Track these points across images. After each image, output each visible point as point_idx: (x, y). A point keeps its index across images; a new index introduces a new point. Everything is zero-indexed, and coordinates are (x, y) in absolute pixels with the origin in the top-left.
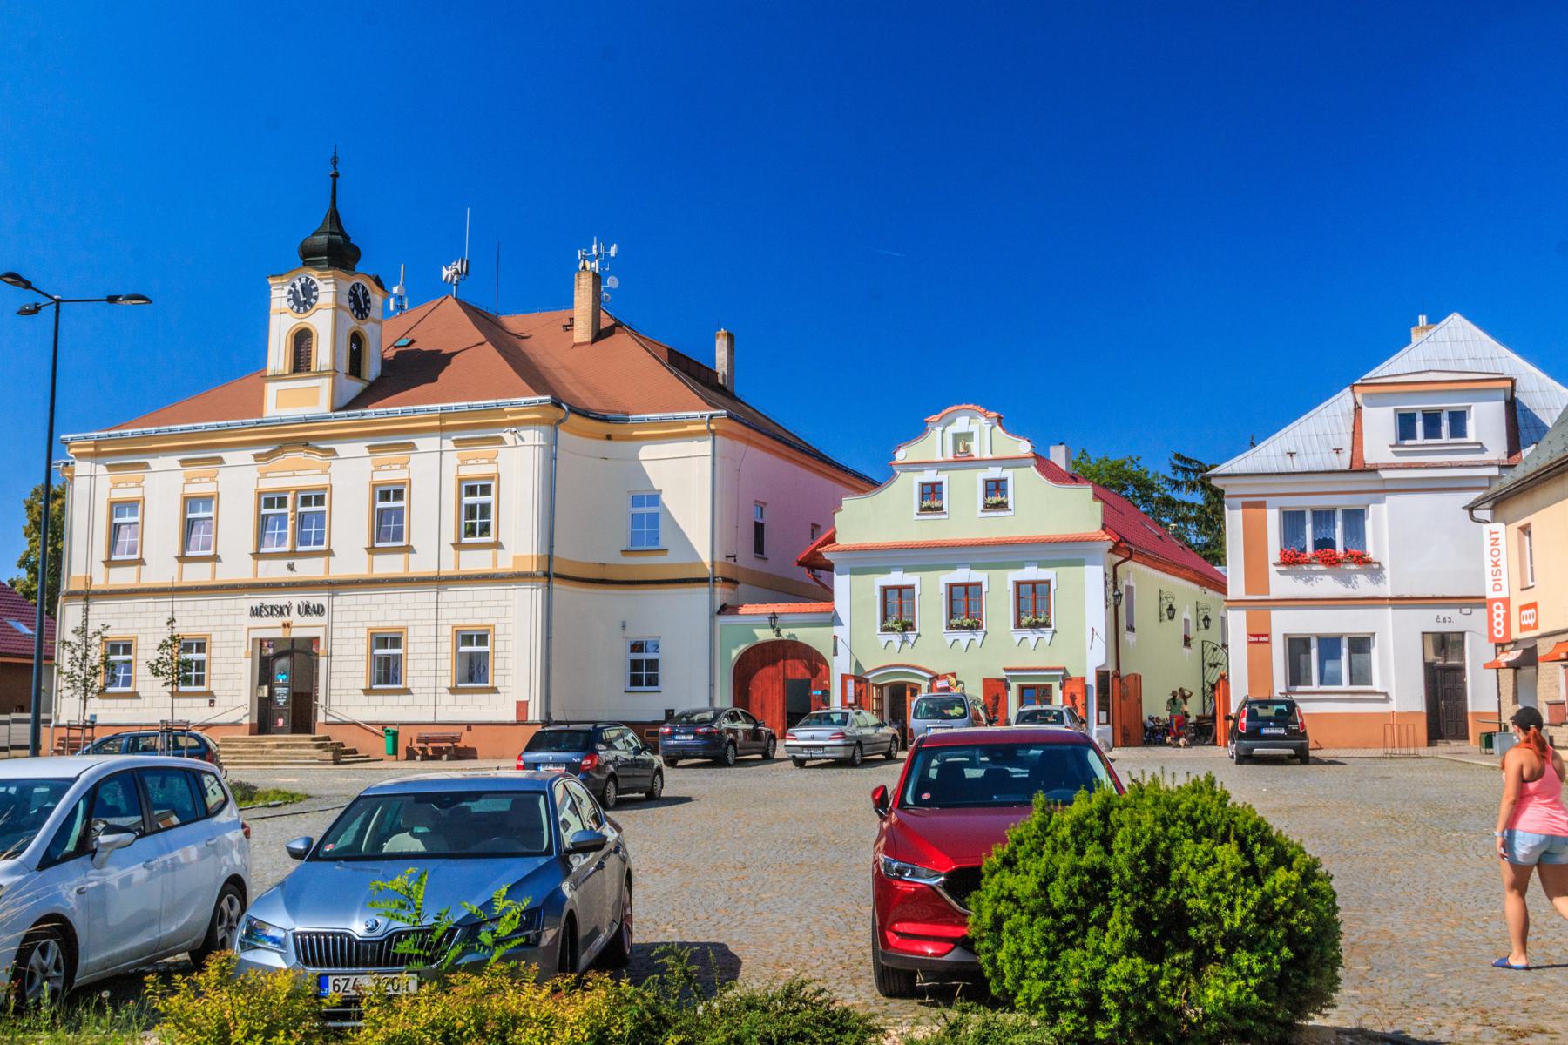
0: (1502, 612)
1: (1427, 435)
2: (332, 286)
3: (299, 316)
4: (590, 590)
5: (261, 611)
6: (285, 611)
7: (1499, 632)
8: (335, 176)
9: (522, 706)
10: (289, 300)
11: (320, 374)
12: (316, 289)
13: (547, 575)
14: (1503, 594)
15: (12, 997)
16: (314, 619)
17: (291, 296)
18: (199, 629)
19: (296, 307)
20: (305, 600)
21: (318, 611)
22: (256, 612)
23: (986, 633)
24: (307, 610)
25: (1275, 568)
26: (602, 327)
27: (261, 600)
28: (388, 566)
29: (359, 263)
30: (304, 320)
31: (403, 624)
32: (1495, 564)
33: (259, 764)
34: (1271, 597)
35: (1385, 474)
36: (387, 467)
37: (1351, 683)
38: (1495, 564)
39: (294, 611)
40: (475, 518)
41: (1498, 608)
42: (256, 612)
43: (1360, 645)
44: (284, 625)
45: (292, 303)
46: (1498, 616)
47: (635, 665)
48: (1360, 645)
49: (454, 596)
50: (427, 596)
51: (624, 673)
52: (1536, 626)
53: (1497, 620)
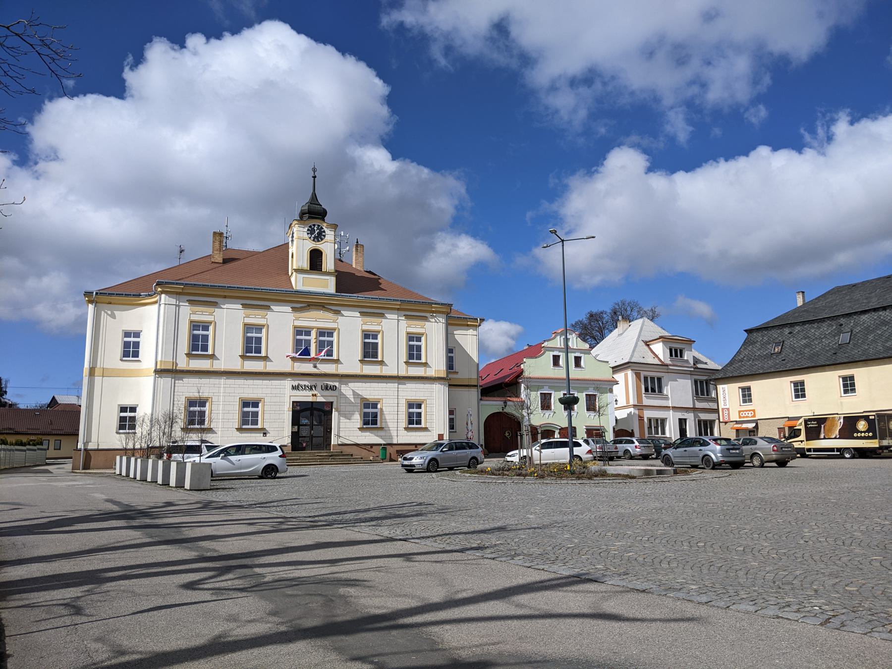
0: (727, 412)
1: (675, 357)
2: (333, 232)
3: (314, 243)
5: (298, 387)
7: (726, 418)
8: (314, 177)
9: (441, 437)
11: (328, 274)
13: (103, 376)
14: (727, 407)
22: (294, 388)
23: (578, 413)
25: (644, 395)
27: (299, 382)
28: (371, 370)
30: (317, 245)
31: (380, 397)
32: (724, 398)
34: (644, 405)
35: (671, 367)
36: (201, 313)
37: (661, 434)
38: (724, 398)
39: (319, 387)
40: (255, 346)
41: (751, 413)
42: (294, 388)
43: (663, 421)
44: (313, 395)
46: (748, 414)
48: (663, 421)
49: (411, 386)
50: (393, 386)
51: (115, 423)
52: (754, 416)
53: (747, 413)
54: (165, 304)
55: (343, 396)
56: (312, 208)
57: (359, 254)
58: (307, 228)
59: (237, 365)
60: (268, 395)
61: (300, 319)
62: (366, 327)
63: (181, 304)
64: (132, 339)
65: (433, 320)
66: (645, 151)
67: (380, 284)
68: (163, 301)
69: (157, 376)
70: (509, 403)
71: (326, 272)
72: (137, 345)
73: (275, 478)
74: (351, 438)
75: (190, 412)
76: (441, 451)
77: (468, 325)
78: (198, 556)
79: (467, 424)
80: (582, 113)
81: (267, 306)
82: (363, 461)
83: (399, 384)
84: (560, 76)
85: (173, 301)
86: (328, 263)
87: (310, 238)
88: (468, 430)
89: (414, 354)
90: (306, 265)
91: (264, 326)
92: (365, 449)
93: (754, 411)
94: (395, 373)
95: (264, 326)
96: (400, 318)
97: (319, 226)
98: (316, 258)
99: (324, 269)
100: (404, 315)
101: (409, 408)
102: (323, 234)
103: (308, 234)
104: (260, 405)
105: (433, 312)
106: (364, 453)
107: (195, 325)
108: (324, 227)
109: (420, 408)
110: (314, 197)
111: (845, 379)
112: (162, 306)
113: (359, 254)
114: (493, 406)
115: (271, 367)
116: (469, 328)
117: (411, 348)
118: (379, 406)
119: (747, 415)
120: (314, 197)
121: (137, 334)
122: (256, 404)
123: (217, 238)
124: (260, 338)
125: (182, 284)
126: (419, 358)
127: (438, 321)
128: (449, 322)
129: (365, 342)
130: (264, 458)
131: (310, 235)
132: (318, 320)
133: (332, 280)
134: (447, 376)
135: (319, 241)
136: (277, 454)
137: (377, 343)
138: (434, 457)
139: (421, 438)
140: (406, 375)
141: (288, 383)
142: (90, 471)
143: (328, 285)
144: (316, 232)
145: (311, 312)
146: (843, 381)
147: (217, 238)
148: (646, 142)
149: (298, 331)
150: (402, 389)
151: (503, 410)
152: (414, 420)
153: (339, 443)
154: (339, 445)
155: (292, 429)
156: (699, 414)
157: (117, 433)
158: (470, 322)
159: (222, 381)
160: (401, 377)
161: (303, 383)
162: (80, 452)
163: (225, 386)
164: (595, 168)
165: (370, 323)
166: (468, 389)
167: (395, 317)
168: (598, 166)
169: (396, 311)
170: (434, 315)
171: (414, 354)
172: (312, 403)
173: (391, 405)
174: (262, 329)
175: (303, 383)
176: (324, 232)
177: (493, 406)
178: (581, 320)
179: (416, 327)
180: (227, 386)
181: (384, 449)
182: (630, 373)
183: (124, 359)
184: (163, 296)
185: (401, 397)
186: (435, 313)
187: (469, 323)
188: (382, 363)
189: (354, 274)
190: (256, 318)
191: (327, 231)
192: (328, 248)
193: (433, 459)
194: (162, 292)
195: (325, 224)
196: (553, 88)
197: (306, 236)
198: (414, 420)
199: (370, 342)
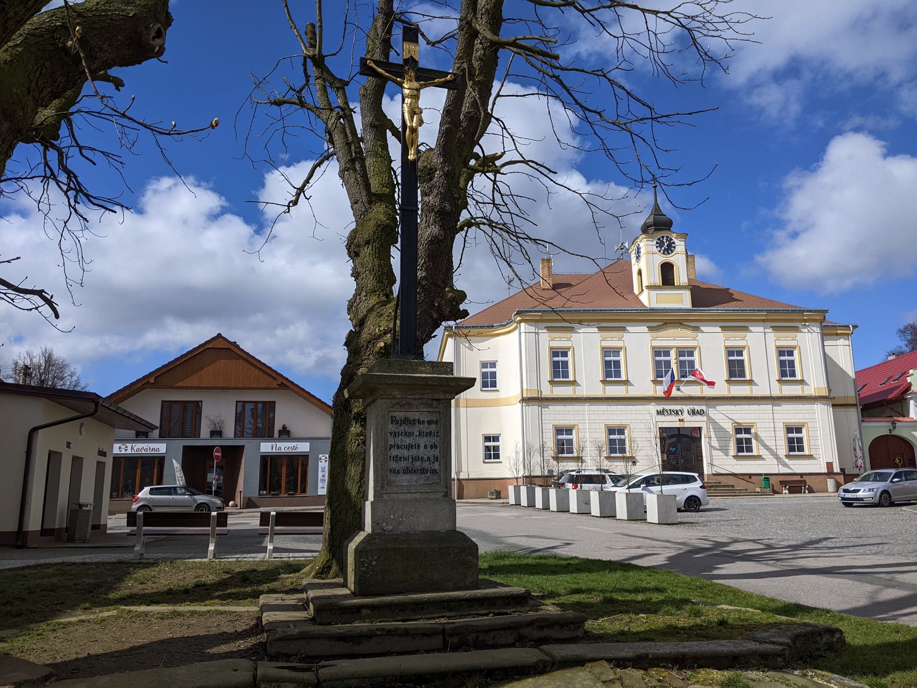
3: (665, 256)
4: (738, 407)
5: (663, 412)
6: (680, 413)
9: (830, 465)
15: (810, 628)
16: (698, 417)
18: (612, 421)
20: (692, 407)
21: (701, 413)
22: (659, 413)
24: (693, 413)
29: (347, 233)
31: (753, 421)
33: (723, 496)
36: (559, 339)
39: (686, 413)
42: (659, 413)
44: (680, 420)
47: (487, 448)
49: (786, 407)
50: (767, 408)
51: (481, 452)
54: (526, 333)
55: (712, 421)
56: (657, 219)
57: (690, 266)
58: (655, 242)
59: (598, 390)
60: (581, 422)
61: (657, 339)
62: (729, 343)
63: (540, 331)
64: (489, 370)
65: (806, 331)
66: (876, 134)
67: (733, 294)
68: (523, 330)
69: (524, 404)
70: (898, 424)
71: (680, 286)
72: (494, 375)
73: (698, 511)
74: (725, 467)
75: (558, 440)
76: (891, 482)
77: (837, 334)
79: (855, 450)
80: (795, 108)
81: (622, 327)
82: (745, 493)
83: (773, 405)
84: (760, 71)
85: (532, 329)
86: (681, 276)
87: (660, 251)
88: (856, 457)
89: (787, 370)
90: (658, 280)
91: (621, 348)
92: (743, 479)
94: (767, 394)
95: (621, 348)
96: (766, 330)
97: (667, 237)
98: (667, 270)
99: (677, 283)
100: (771, 327)
101: (610, 434)
102: (673, 245)
103: (657, 247)
104: (574, 432)
105: (805, 321)
106: (740, 485)
107: (555, 353)
108: (673, 238)
109: (623, 434)
112: (523, 335)
113: (690, 266)
114: (879, 428)
115: (633, 392)
116: (838, 337)
117: (782, 364)
118: (753, 431)
121: (493, 365)
122: (799, 430)
123: (546, 264)
124: (619, 362)
125: (540, 311)
126: (793, 374)
127: (811, 331)
128: (824, 332)
129: (729, 360)
130: (685, 489)
131: (659, 249)
132: (676, 339)
133: (687, 295)
134: (829, 395)
135: (669, 254)
136: (697, 484)
137: (743, 361)
138: (886, 489)
139: (806, 466)
140: (701, 395)
141: (653, 408)
142: (463, 501)
143: (684, 300)
144: (666, 244)
145: (668, 331)
147: (546, 264)
148: (870, 122)
149: (657, 352)
150: (777, 412)
151: (890, 432)
152: (795, 446)
153: (714, 472)
154: (714, 475)
156: (913, 432)
157: (484, 462)
158: (840, 330)
159: (586, 407)
160: (775, 397)
161: (667, 407)
163: (589, 412)
164: (815, 164)
165: (733, 339)
166: (844, 409)
167: (761, 329)
168: (818, 162)
169: (762, 323)
170: (807, 324)
171: (787, 370)
172: (678, 428)
173: (766, 429)
174: (619, 352)
175: (667, 407)
176: (674, 243)
177: (879, 428)
178: (912, 323)
179: (786, 339)
180: (582, 413)
181: (767, 479)
183: (484, 389)
184: (523, 324)
185: (778, 421)
186: (808, 322)
187: (838, 332)
188: (751, 382)
189: (699, 286)
190: (612, 340)
191: (677, 242)
192: (678, 259)
193: (885, 492)
194: (520, 322)
195: (674, 235)
196: (754, 84)
197: (655, 250)
198: (795, 446)
199: (735, 360)
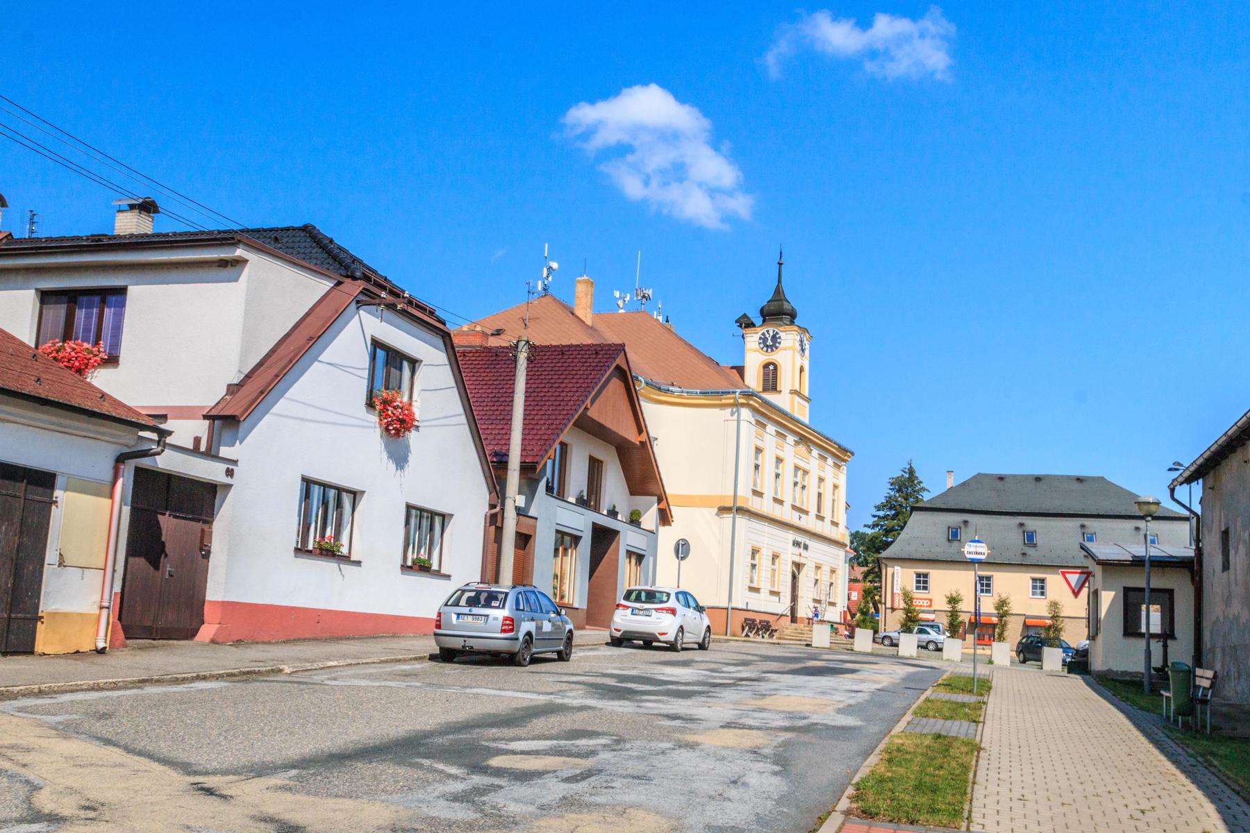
0: (925, 604)
8: (780, 264)
10: (760, 343)
12: (780, 338)
17: (761, 341)
19: (765, 349)
26: (159, 516)
30: (771, 357)
45: (762, 345)
46: (923, 603)
52: (930, 606)
53: (921, 602)
78: (1100, 618)
93: (931, 600)
110: (778, 291)
111: (918, 575)
119: (921, 603)
120: (778, 291)
146: (917, 577)
155: (850, 574)
162: (1142, 593)
182: (212, 453)
